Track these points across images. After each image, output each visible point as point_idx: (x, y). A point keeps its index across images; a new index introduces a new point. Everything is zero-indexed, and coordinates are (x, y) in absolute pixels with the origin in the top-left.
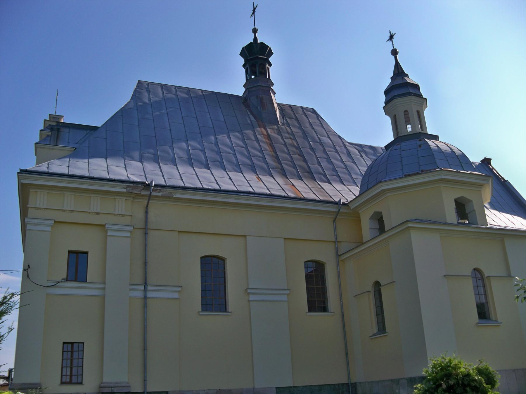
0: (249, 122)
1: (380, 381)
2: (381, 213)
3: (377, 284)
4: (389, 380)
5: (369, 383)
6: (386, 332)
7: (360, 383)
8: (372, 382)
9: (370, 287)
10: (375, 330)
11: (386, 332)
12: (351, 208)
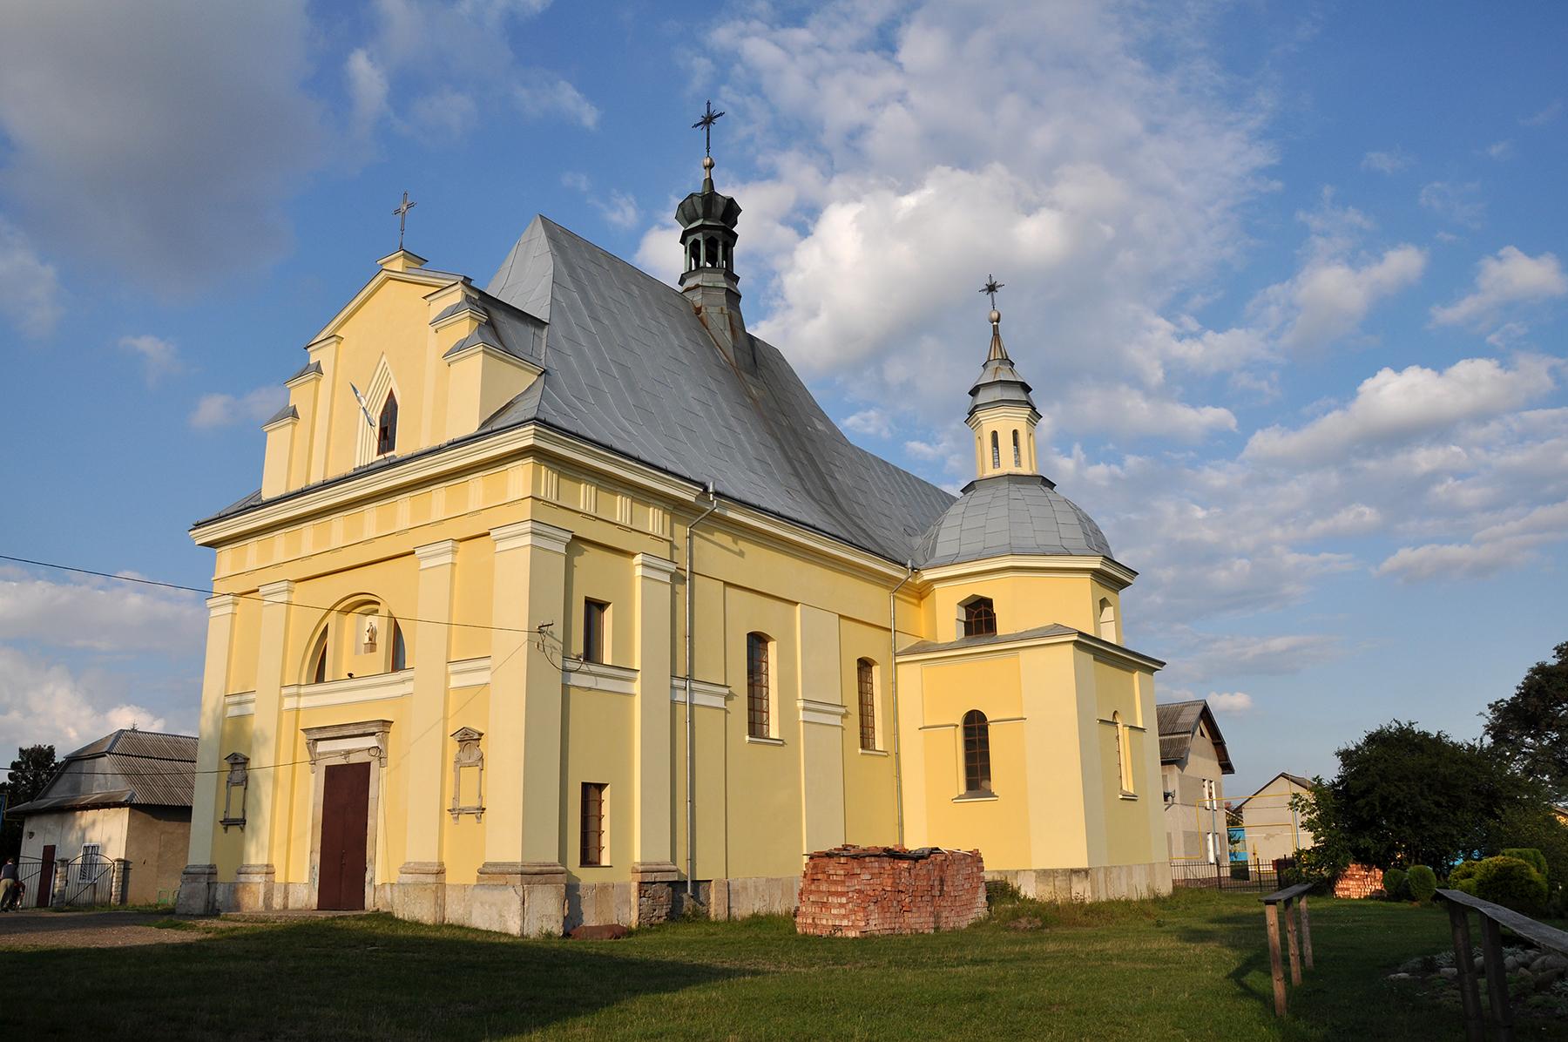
10: (963, 790)
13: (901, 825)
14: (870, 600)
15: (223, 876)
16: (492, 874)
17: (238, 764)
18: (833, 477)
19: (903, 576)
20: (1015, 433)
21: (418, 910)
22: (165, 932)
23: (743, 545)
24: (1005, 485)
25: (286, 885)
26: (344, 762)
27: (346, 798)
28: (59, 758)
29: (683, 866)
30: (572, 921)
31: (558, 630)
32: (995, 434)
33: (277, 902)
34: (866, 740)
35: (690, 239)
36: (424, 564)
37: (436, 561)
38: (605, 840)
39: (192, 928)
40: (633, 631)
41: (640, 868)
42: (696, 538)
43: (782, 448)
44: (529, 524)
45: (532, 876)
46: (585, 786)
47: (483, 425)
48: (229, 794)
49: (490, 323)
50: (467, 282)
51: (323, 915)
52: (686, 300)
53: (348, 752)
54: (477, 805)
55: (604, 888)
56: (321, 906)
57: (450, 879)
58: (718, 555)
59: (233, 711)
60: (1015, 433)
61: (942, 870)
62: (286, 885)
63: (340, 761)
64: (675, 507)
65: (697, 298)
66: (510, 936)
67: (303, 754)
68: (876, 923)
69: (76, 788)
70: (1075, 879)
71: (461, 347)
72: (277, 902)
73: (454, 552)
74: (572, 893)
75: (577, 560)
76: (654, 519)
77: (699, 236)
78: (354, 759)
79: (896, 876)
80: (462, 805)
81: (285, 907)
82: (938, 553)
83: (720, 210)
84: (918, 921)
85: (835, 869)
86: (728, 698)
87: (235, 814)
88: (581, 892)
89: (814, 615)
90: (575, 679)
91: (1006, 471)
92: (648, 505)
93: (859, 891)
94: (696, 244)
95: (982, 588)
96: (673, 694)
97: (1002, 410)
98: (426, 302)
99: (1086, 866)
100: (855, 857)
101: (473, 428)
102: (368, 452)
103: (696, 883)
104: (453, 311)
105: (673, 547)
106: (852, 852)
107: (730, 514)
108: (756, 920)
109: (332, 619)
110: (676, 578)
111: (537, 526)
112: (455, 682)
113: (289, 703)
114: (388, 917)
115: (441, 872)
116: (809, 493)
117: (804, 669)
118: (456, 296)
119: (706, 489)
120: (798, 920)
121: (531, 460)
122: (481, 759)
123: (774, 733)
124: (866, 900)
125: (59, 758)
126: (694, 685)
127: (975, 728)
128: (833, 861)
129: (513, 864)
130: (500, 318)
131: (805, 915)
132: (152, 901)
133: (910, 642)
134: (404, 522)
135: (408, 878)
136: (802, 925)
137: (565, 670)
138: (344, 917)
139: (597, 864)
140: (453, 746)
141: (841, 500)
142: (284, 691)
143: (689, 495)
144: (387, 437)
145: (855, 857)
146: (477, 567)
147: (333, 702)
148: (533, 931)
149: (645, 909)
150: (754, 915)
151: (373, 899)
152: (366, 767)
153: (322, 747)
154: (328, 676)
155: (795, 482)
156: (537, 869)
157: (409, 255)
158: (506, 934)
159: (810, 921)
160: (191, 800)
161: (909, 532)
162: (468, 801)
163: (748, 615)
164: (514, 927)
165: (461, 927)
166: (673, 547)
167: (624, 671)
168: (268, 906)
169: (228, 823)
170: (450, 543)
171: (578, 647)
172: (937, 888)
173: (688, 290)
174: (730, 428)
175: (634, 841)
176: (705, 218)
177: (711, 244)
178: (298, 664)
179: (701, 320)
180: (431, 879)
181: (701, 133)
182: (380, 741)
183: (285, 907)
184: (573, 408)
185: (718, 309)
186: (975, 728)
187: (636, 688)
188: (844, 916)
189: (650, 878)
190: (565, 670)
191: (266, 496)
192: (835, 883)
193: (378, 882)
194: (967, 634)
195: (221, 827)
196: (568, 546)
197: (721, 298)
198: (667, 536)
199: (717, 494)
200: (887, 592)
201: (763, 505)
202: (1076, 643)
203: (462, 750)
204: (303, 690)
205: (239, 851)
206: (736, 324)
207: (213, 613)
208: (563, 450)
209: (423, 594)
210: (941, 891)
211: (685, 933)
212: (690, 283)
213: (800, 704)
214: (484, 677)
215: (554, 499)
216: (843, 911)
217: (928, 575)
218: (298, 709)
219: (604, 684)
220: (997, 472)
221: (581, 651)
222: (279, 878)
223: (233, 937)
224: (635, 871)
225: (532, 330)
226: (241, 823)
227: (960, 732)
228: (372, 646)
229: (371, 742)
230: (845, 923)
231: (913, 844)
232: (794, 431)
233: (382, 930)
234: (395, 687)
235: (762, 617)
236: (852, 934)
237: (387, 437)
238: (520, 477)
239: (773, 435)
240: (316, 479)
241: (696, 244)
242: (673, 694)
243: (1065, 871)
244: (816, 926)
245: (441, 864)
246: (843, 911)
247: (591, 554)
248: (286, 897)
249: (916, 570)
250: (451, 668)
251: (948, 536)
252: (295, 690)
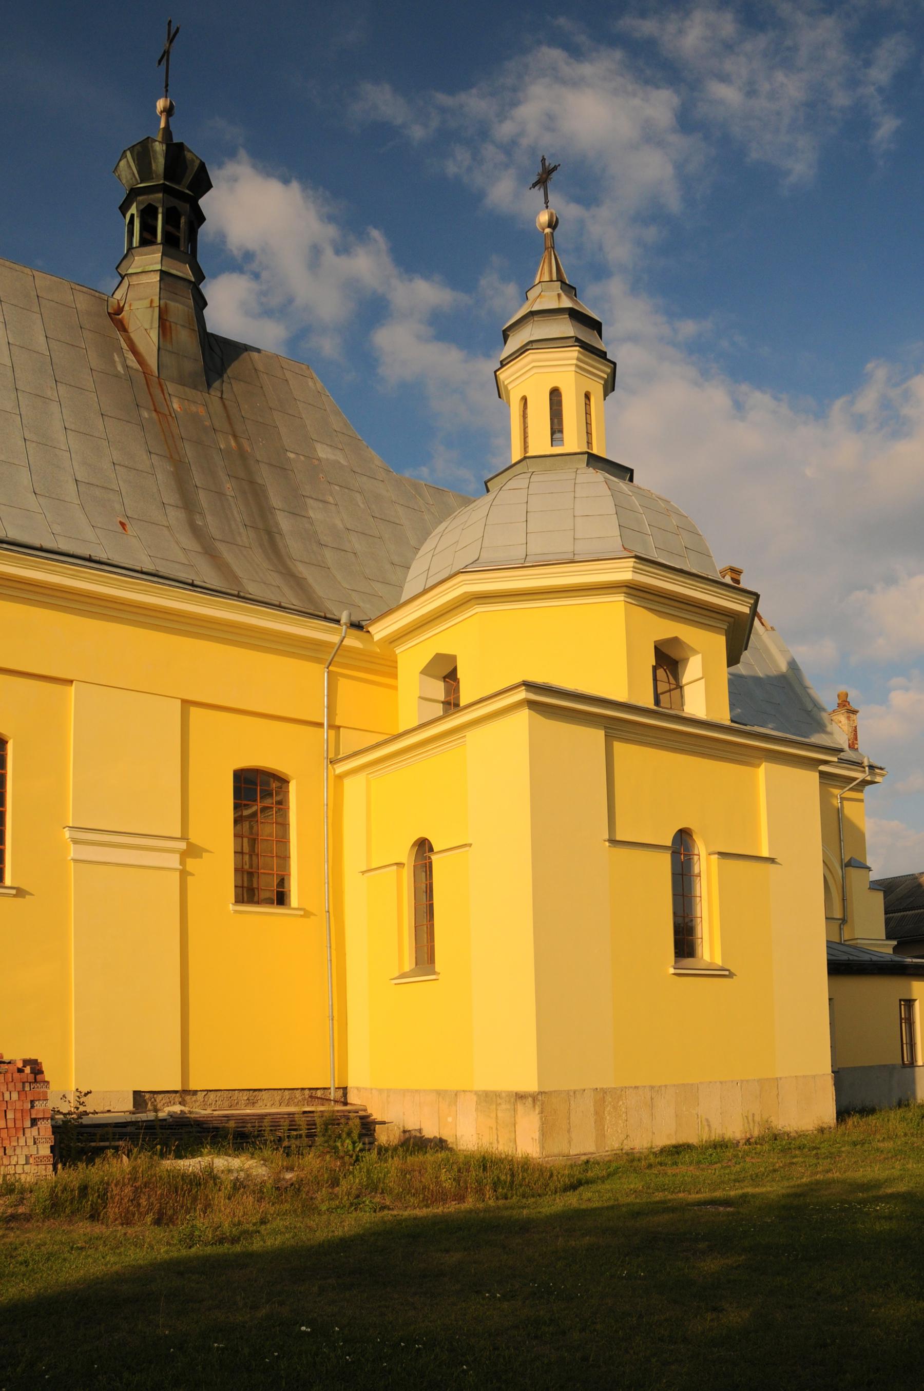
0: (120, 368)
1: (408, 1090)
2: (453, 658)
3: (423, 847)
4: (432, 1091)
5: (380, 1091)
6: (434, 972)
7: (358, 1089)
8: (389, 1090)
9: (404, 853)
10: (408, 964)
11: (434, 972)
12: (376, 638)
14: (293, 684)
19: (336, 639)
20: (555, 395)
32: (525, 400)
60: (555, 395)
70: (520, 1108)
99: (532, 1086)
185: (147, 303)
202: (532, 705)
243: (509, 1094)
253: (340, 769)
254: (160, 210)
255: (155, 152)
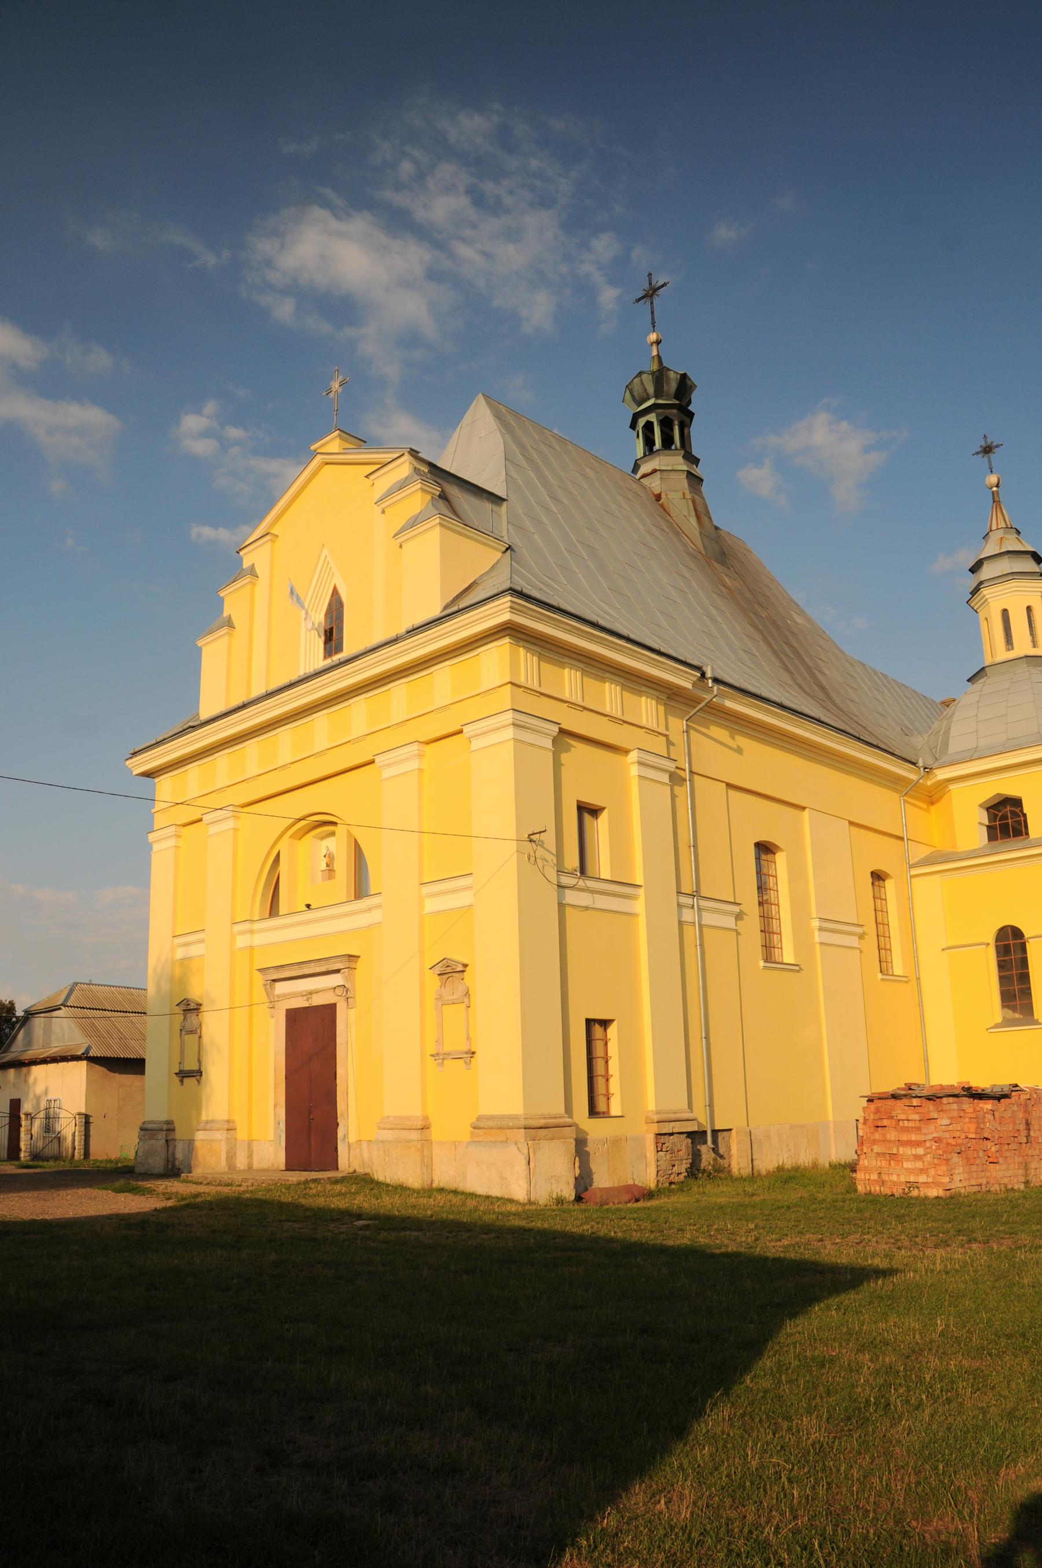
13: (926, 1060)
14: (880, 804)
15: (179, 1134)
16: (488, 1129)
17: (190, 1008)
18: (822, 673)
19: (913, 777)
20: (1029, 609)
21: (400, 1170)
22: (122, 1197)
23: (741, 741)
24: (1023, 667)
25: (250, 1143)
26: (306, 1004)
27: (312, 1042)
28: (19, 1013)
29: (702, 1119)
30: (583, 1182)
31: (549, 839)
32: (1005, 612)
33: (241, 1162)
34: (884, 965)
35: (642, 422)
36: (386, 773)
37: (399, 768)
38: (614, 1086)
39: (151, 1192)
40: (631, 839)
41: (656, 1118)
42: (692, 732)
43: (765, 639)
44: (510, 715)
45: (538, 1130)
46: (589, 1022)
47: (445, 608)
48: (182, 1043)
49: (443, 497)
50: (414, 453)
51: (295, 1177)
52: (644, 487)
53: (311, 993)
54: (464, 1047)
55: (616, 1143)
56: (289, 1167)
57: (436, 1134)
58: (716, 751)
59: (180, 953)
61: (1027, 1112)
62: (250, 1143)
63: (300, 1003)
64: (671, 697)
65: (655, 484)
66: (517, 1202)
67: (259, 994)
68: (960, 1179)
69: (29, 1042)
71: (413, 523)
72: (241, 1162)
73: (421, 756)
74: (581, 1144)
75: (564, 757)
76: (647, 709)
77: (652, 417)
78: (317, 1001)
79: (978, 1119)
80: (447, 1048)
81: (250, 1167)
82: (952, 748)
83: (673, 386)
84: (1006, 1175)
85: (899, 1109)
86: (739, 917)
87: (190, 1065)
88: (590, 1148)
89: (828, 821)
90: (571, 897)
91: (1022, 654)
92: (639, 693)
93: (937, 1140)
94: (649, 427)
95: (1008, 786)
96: (680, 914)
97: (1013, 584)
98: (368, 482)
100: (929, 1098)
101: (436, 612)
102: (314, 656)
103: (715, 1132)
104: (402, 485)
105: (669, 743)
106: (925, 1093)
107: (729, 704)
108: (786, 1177)
109: (283, 846)
110: (676, 779)
111: (519, 716)
112: (430, 906)
113: (241, 941)
114: (365, 1181)
115: (425, 1128)
116: (801, 687)
117: (814, 879)
118: (404, 468)
119: (703, 675)
120: (859, 1175)
121: (507, 640)
122: (467, 994)
123: (788, 956)
124: (950, 1150)
125: (19, 1013)
126: (702, 903)
127: (1011, 947)
128: (900, 1104)
129: (515, 1117)
130: (454, 491)
131: (867, 1169)
132: (113, 1156)
133: (924, 852)
134: (359, 728)
135: (387, 1135)
136: (865, 1182)
137: (560, 886)
138: (319, 1191)
139: (606, 1115)
140: (433, 981)
141: (834, 695)
142: (236, 928)
143: (685, 680)
144: (332, 638)
145: (929, 1098)
146: (453, 771)
147: (289, 938)
148: (542, 1195)
149: (664, 1165)
150: (780, 1169)
151: (348, 1160)
152: (331, 1008)
153: (281, 988)
154: (283, 908)
155: (785, 676)
156: (541, 1122)
157: (346, 434)
158: (511, 1201)
159: (874, 1177)
160: (144, 1049)
161: (906, 732)
162: (455, 1043)
163: (758, 822)
164: (519, 1191)
165: (455, 1192)
166: (669, 743)
167: (625, 886)
168: (231, 1166)
169: (184, 1075)
170: (415, 747)
171: (572, 861)
172: (1024, 1133)
173: (644, 476)
174: (712, 619)
175: (646, 1089)
176: (657, 397)
177: (666, 424)
178: (254, 900)
179: (662, 506)
180: (415, 1135)
181: (645, 307)
182: (347, 979)
183: (250, 1167)
184: (548, 586)
185: (680, 494)
186: (1011, 947)
187: (639, 906)
188: (922, 1171)
189: (667, 1128)
190: (560, 886)
191: (204, 715)
192: (907, 1130)
193: (352, 1139)
194: (990, 839)
195: (176, 1079)
196: (555, 741)
197: (683, 482)
198: (662, 730)
199: (716, 680)
200: (895, 796)
201: (764, 695)
203: (443, 985)
204: (256, 926)
205: (196, 1104)
206: (701, 513)
207: (155, 848)
208: (543, 626)
209: (388, 806)
210: (1028, 1136)
211: (717, 1194)
212: (645, 469)
213: (816, 924)
214: (465, 899)
215: (536, 687)
216: (919, 1165)
217: (941, 774)
218: (252, 948)
219: (602, 902)
220: (1011, 655)
221: (576, 864)
222: (241, 1134)
223: (192, 1206)
224: (649, 1121)
225: (488, 506)
226: (197, 1074)
227: (992, 951)
228: (330, 871)
229: (336, 980)
230: (923, 1179)
231: (946, 1074)
232: (774, 623)
233: (363, 1202)
234: (360, 917)
235: (768, 823)
236: (933, 1193)
237: (332, 638)
238: (497, 661)
239: (755, 627)
240: (256, 693)
241: (649, 427)
242: (680, 914)
244: (883, 1183)
245: (426, 1118)
246: (919, 1165)
247: (580, 749)
248: (250, 1156)
249: (928, 770)
250: (425, 890)
251: (962, 730)
252: (246, 926)
253: (914, 872)
254: (676, 422)
255: (668, 378)
